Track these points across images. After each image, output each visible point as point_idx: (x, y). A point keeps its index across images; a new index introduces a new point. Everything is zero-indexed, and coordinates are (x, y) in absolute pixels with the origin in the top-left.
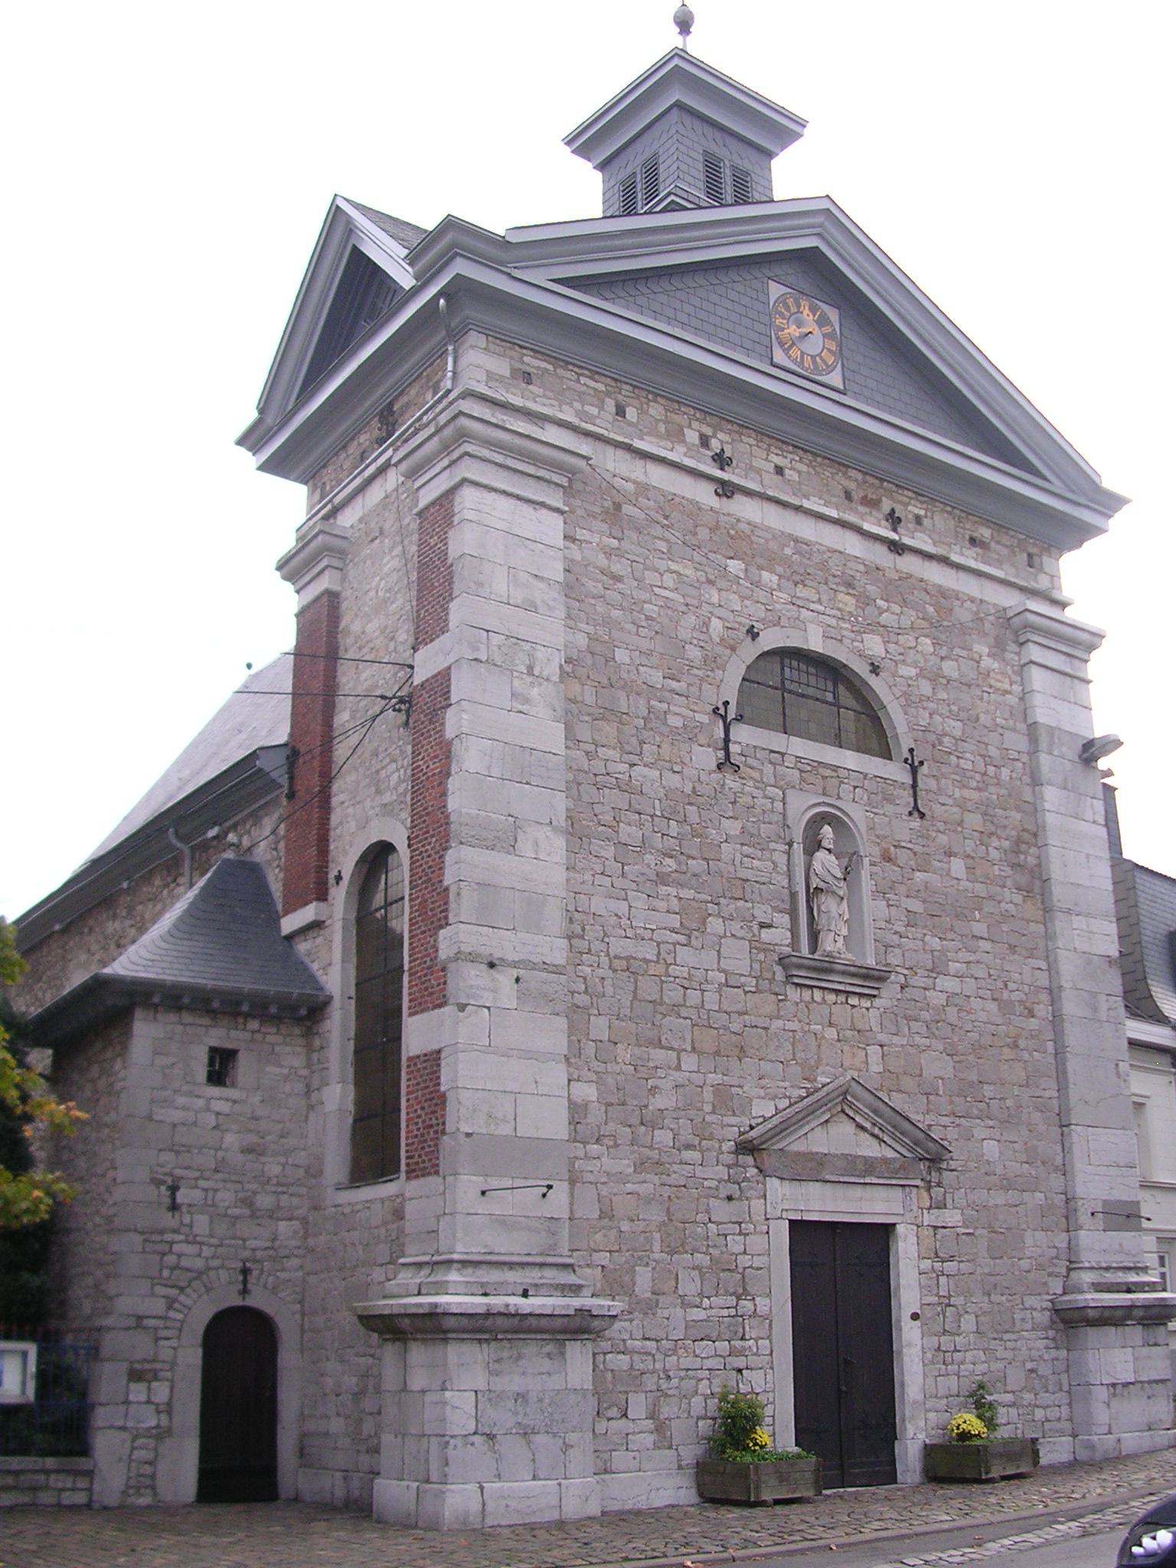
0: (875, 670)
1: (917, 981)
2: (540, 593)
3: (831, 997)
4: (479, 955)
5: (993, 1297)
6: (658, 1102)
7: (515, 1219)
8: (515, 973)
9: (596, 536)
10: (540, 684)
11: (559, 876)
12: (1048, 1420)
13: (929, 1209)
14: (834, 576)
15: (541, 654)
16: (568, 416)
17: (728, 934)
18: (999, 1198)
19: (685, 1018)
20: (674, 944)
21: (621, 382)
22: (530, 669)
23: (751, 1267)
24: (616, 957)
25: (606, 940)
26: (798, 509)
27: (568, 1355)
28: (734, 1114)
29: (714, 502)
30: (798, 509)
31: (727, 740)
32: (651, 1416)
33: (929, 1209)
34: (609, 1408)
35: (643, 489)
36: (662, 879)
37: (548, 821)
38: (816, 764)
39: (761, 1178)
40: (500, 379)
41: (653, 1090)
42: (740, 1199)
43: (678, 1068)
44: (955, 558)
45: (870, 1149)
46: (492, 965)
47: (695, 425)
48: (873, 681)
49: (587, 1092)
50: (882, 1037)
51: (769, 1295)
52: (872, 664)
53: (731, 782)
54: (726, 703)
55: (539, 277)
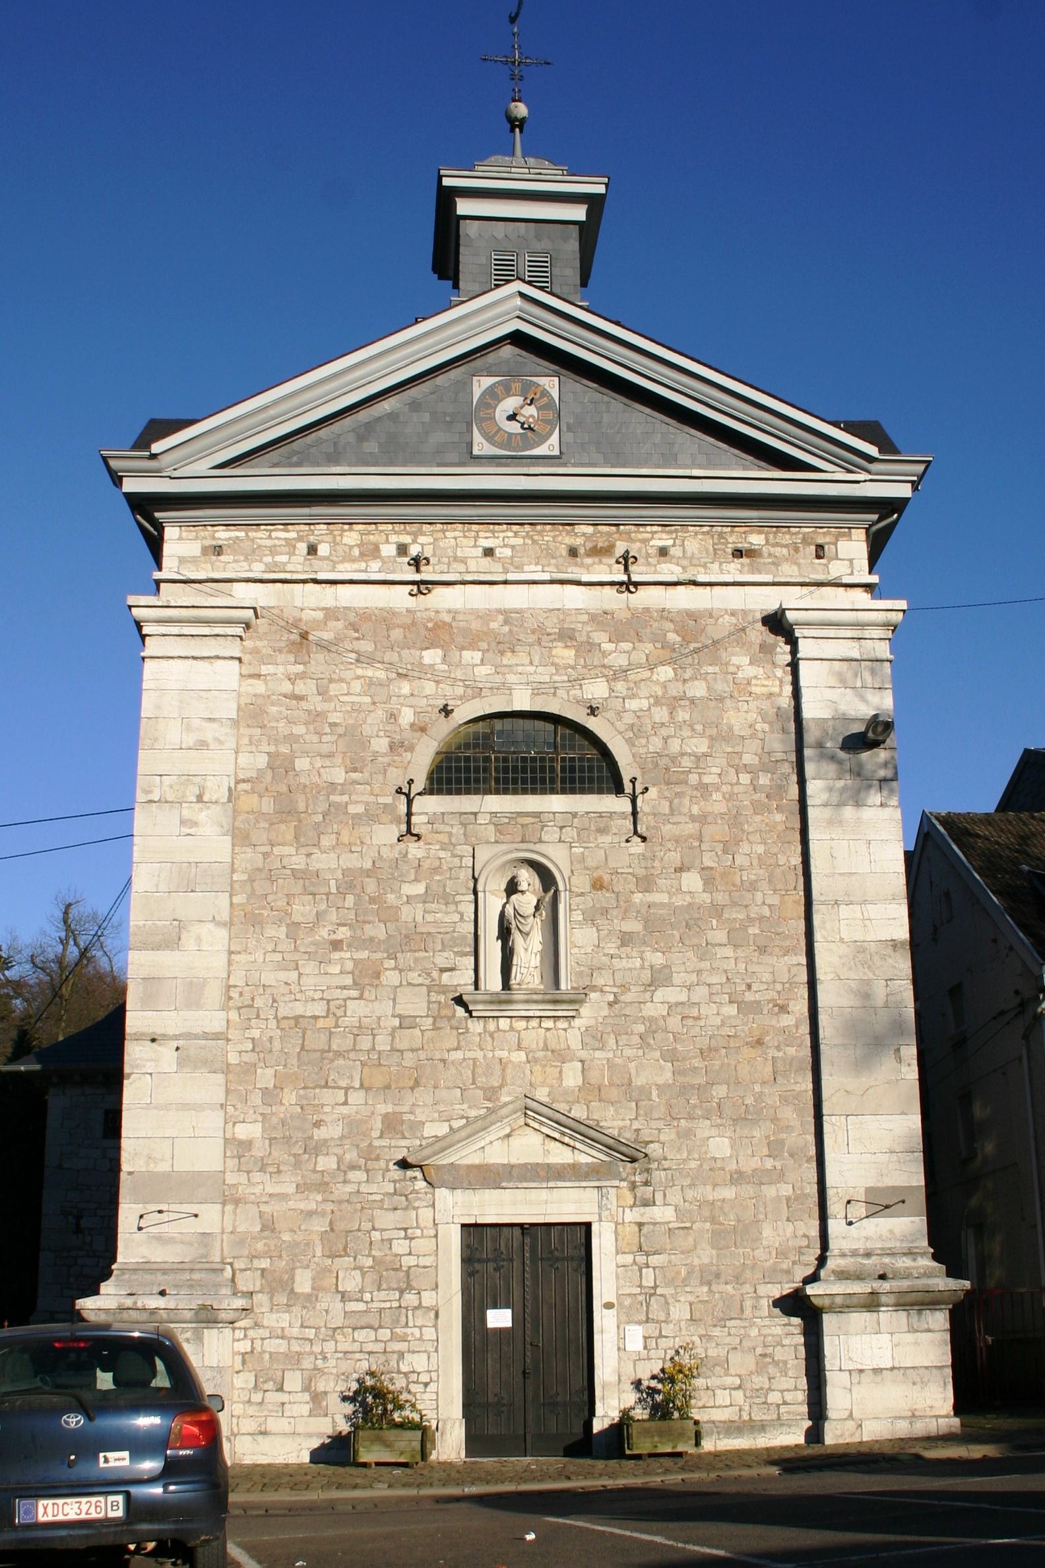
0: (593, 711)
1: (628, 997)
2: (210, 732)
3: (521, 1024)
4: (143, 1034)
5: (714, 1288)
6: (320, 1134)
7: (170, 1235)
8: (175, 1044)
9: (280, 669)
10: (208, 808)
11: (219, 962)
12: (785, 1403)
13: (631, 1207)
14: (549, 634)
15: (210, 783)
16: (258, 571)
17: (404, 983)
18: (728, 1193)
19: (355, 1061)
20: (345, 1000)
21: (313, 524)
22: (200, 799)
23: (417, 1266)
24: (285, 1018)
25: (275, 1005)
26: (505, 582)
27: (206, 1341)
28: (404, 1138)
29: (412, 602)
30: (505, 582)
31: (409, 814)
32: (306, 1388)
33: (631, 1207)
34: (265, 1382)
35: (331, 614)
36: (336, 945)
37: (211, 919)
38: (514, 816)
39: (430, 1190)
40: (193, 560)
41: (318, 1124)
42: (406, 1209)
43: (346, 1103)
44: (701, 578)
45: (560, 1155)
46: (153, 1040)
47: (394, 538)
48: (592, 724)
49: (250, 1130)
50: (583, 1054)
51: (436, 1287)
52: (591, 707)
53: (415, 850)
54: (411, 782)
55: (202, 467)
